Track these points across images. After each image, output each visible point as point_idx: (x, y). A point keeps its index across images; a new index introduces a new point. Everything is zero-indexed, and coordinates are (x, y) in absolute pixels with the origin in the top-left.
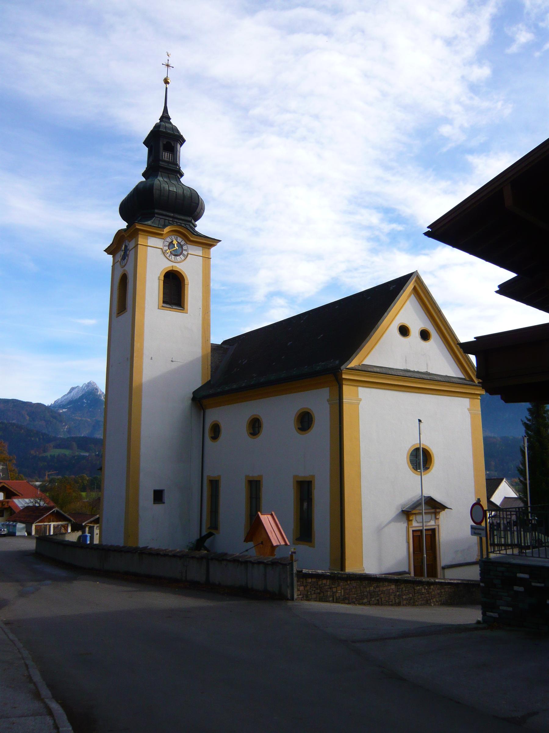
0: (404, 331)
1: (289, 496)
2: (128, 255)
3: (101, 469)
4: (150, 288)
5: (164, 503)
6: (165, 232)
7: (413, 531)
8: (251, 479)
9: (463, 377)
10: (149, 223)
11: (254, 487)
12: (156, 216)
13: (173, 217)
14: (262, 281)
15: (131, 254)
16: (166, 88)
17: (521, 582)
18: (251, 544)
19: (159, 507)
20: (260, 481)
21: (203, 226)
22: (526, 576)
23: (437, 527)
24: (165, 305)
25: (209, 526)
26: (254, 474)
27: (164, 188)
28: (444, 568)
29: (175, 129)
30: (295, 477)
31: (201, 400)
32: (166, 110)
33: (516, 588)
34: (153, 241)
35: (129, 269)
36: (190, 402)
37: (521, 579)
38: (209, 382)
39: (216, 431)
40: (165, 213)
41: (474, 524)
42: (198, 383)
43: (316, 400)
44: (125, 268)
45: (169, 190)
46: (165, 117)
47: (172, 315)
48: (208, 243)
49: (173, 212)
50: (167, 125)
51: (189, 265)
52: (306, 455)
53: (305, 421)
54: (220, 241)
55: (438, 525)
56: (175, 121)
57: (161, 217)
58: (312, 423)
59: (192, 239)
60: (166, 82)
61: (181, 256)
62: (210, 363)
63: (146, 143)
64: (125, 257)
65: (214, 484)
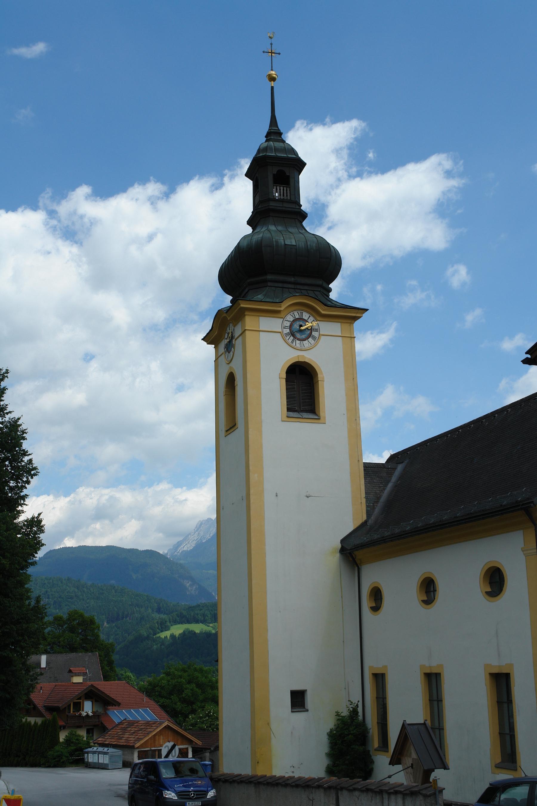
1: (482, 696)
2: (233, 346)
3: (217, 661)
4: (269, 390)
5: (307, 711)
6: (282, 309)
8: (428, 671)
10: (260, 297)
13: (295, 283)
15: (238, 343)
16: (272, 88)
18: (399, 767)
19: (300, 717)
20: (440, 674)
21: (337, 289)
24: (291, 414)
27: (277, 242)
30: (486, 666)
31: (354, 552)
32: (273, 121)
35: (236, 367)
36: (338, 555)
38: (364, 524)
42: (350, 528)
44: (231, 365)
45: (285, 244)
47: (303, 429)
48: (349, 315)
50: (278, 145)
51: (323, 352)
54: (367, 310)
57: (276, 285)
58: (503, 584)
59: (323, 312)
61: (310, 339)
62: (364, 495)
64: (229, 347)
65: (380, 679)
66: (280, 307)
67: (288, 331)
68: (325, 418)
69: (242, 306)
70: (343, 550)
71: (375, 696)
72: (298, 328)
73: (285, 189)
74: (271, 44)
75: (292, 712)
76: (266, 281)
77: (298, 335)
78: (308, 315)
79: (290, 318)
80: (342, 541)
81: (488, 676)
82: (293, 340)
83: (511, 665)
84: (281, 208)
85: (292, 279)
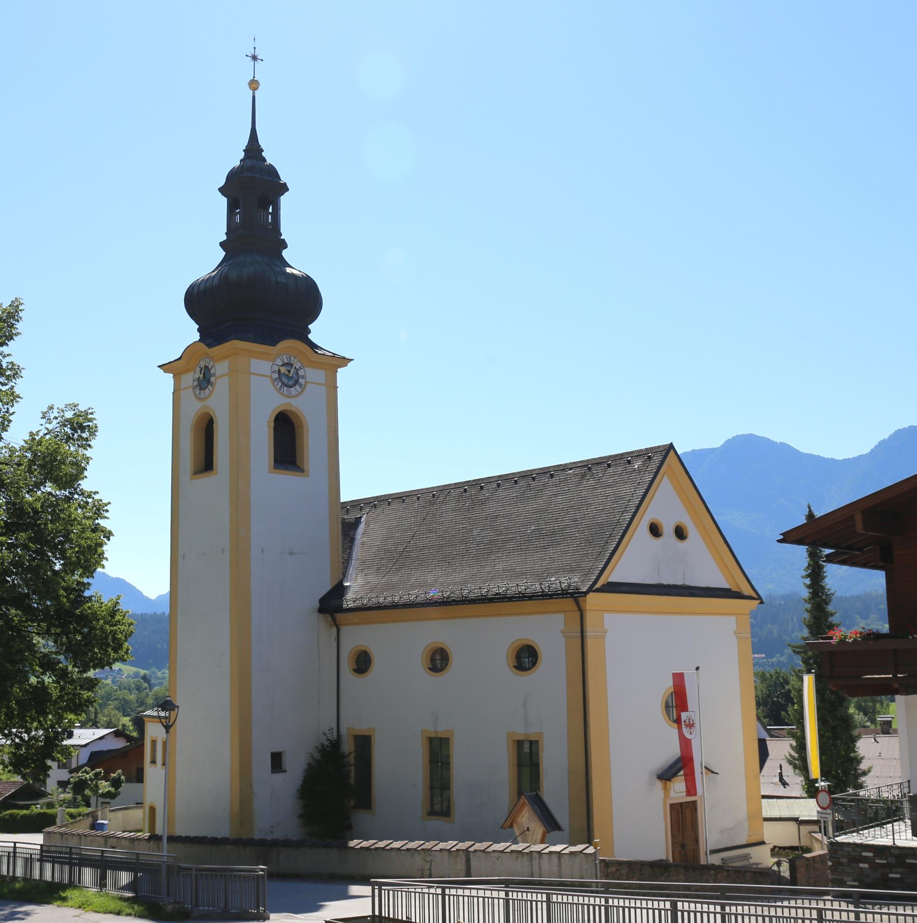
0: (655, 530)
11: (438, 751)
17: (866, 860)
21: (318, 331)
22: (871, 854)
26: (442, 729)
33: (861, 865)
37: (866, 857)
39: (363, 663)
41: (819, 809)
46: (253, 149)
47: (287, 480)
56: (271, 156)
60: (254, 85)
61: (297, 386)
75: (272, 773)
77: (285, 380)
80: (322, 601)
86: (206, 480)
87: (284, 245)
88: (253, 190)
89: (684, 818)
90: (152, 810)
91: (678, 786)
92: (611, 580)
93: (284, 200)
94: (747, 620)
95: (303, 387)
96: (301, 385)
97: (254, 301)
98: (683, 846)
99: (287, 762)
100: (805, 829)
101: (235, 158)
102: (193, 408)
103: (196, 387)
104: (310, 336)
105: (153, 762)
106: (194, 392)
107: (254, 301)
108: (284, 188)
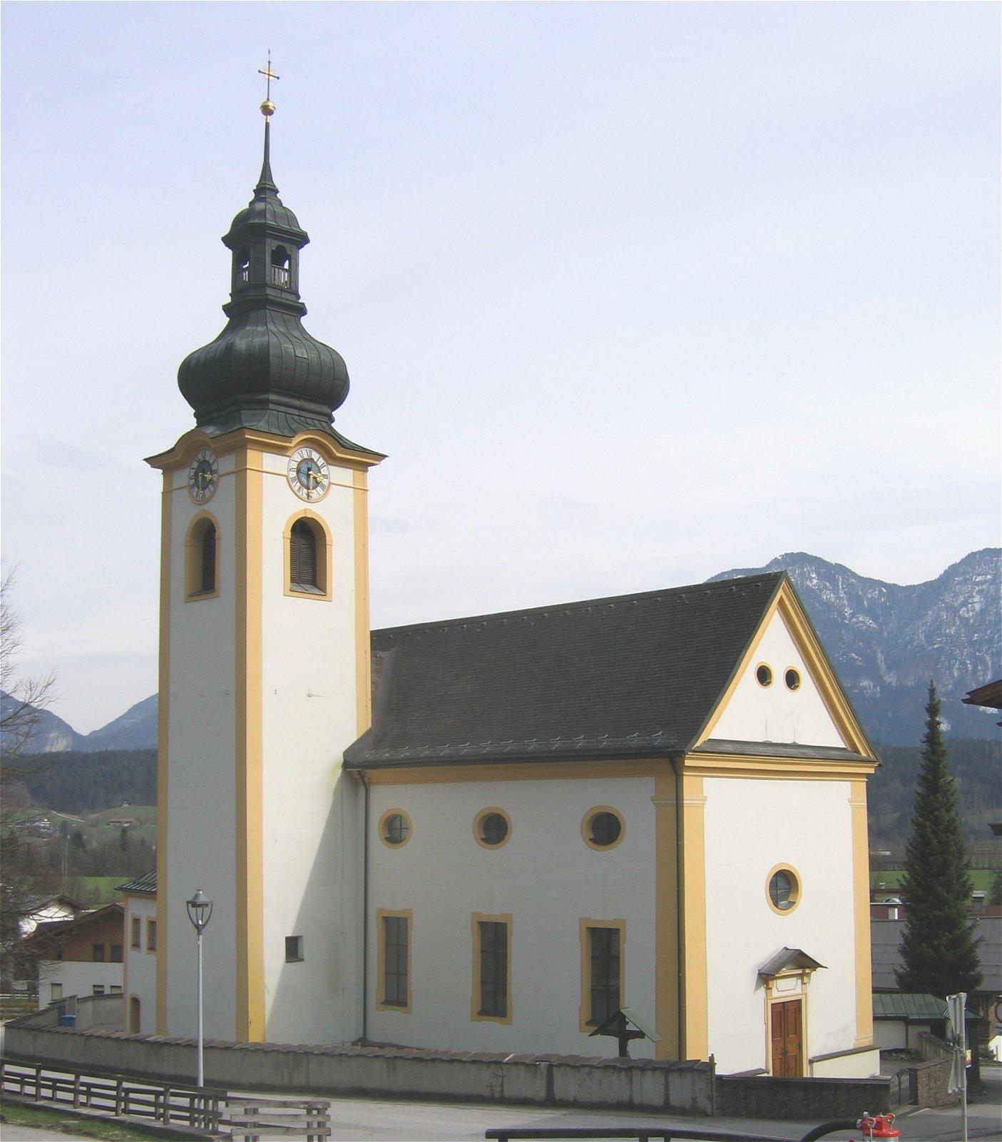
0: (764, 675)
6: (292, 445)
7: (773, 1005)
9: (844, 746)
10: (262, 425)
11: (494, 940)
12: (271, 406)
14: (853, 791)
16: (267, 125)
21: (348, 421)
23: (804, 996)
25: (589, 1018)
28: (811, 1062)
29: (290, 217)
31: (359, 769)
34: (270, 461)
36: (340, 771)
38: (367, 734)
39: (395, 830)
40: (286, 400)
43: (629, 797)
46: (265, 189)
47: (306, 605)
48: (361, 459)
49: (298, 398)
51: (333, 506)
52: (612, 886)
53: (605, 829)
55: (806, 994)
56: (289, 196)
59: (338, 455)
60: (267, 111)
63: (227, 241)
66: (291, 443)
67: (295, 474)
68: (331, 595)
69: (247, 436)
70: (346, 765)
71: (591, 955)
72: (306, 470)
73: (277, 270)
74: (269, 62)
76: (267, 402)
78: (318, 456)
79: (297, 457)
80: (347, 753)
81: (381, 920)
82: (300, 488)
83: (624, 921)
84: (278, 299)
85: (297, 403)
86: (204, 606)
87: (302, 311)
88: (264, 243)
89: (786, 1020)
90: (136, 1002)
91: (786, 988)
92: (711, 737)
93: (304, 254)
94: (862, 786)
95: (326, 490)
96: (323, 487)
97: (260, 381)
98: (785, 1053)
99: (306, 949)
100: (914, 1030)
101: (243, 199)
102: (188, 514)
103: (192, 486)
104: (332, 425)
105: (136, 945)
106: (190, 493)
107: (260, 381)
108: (302, 240)
